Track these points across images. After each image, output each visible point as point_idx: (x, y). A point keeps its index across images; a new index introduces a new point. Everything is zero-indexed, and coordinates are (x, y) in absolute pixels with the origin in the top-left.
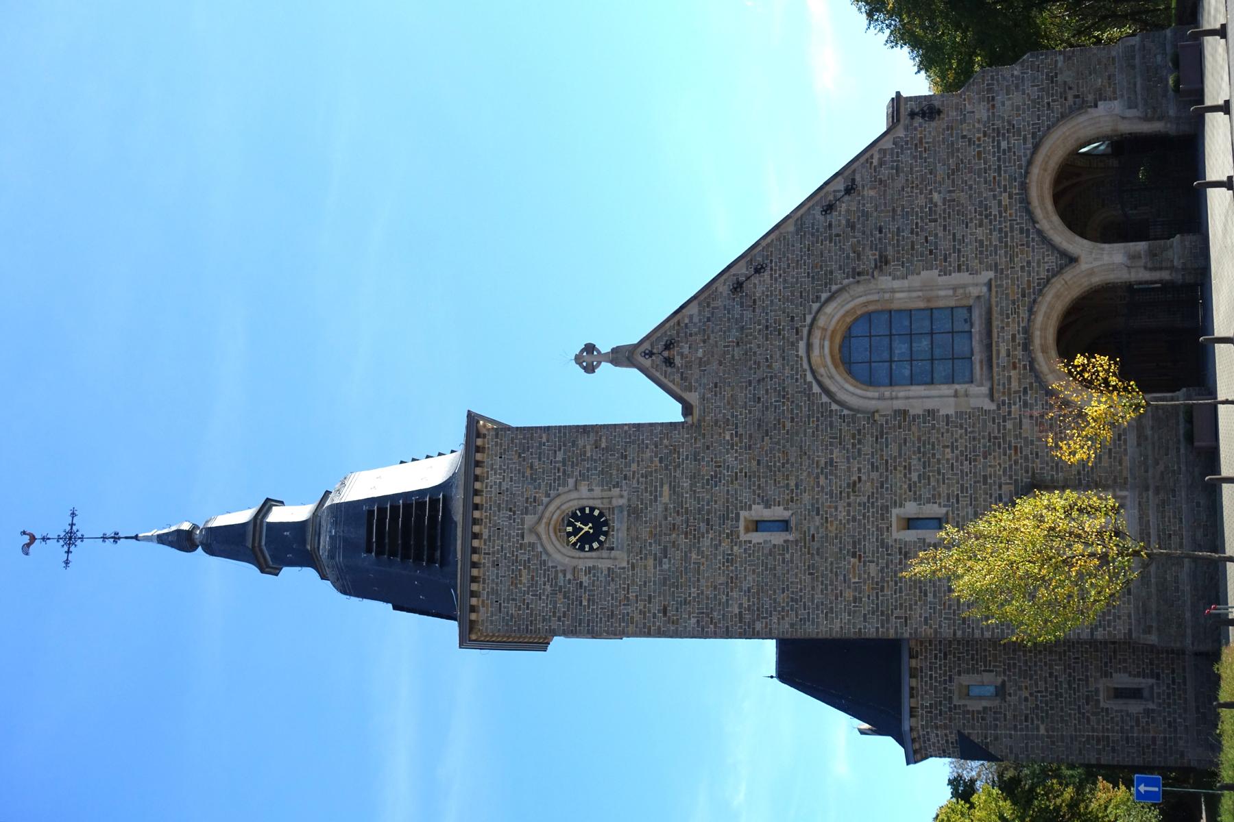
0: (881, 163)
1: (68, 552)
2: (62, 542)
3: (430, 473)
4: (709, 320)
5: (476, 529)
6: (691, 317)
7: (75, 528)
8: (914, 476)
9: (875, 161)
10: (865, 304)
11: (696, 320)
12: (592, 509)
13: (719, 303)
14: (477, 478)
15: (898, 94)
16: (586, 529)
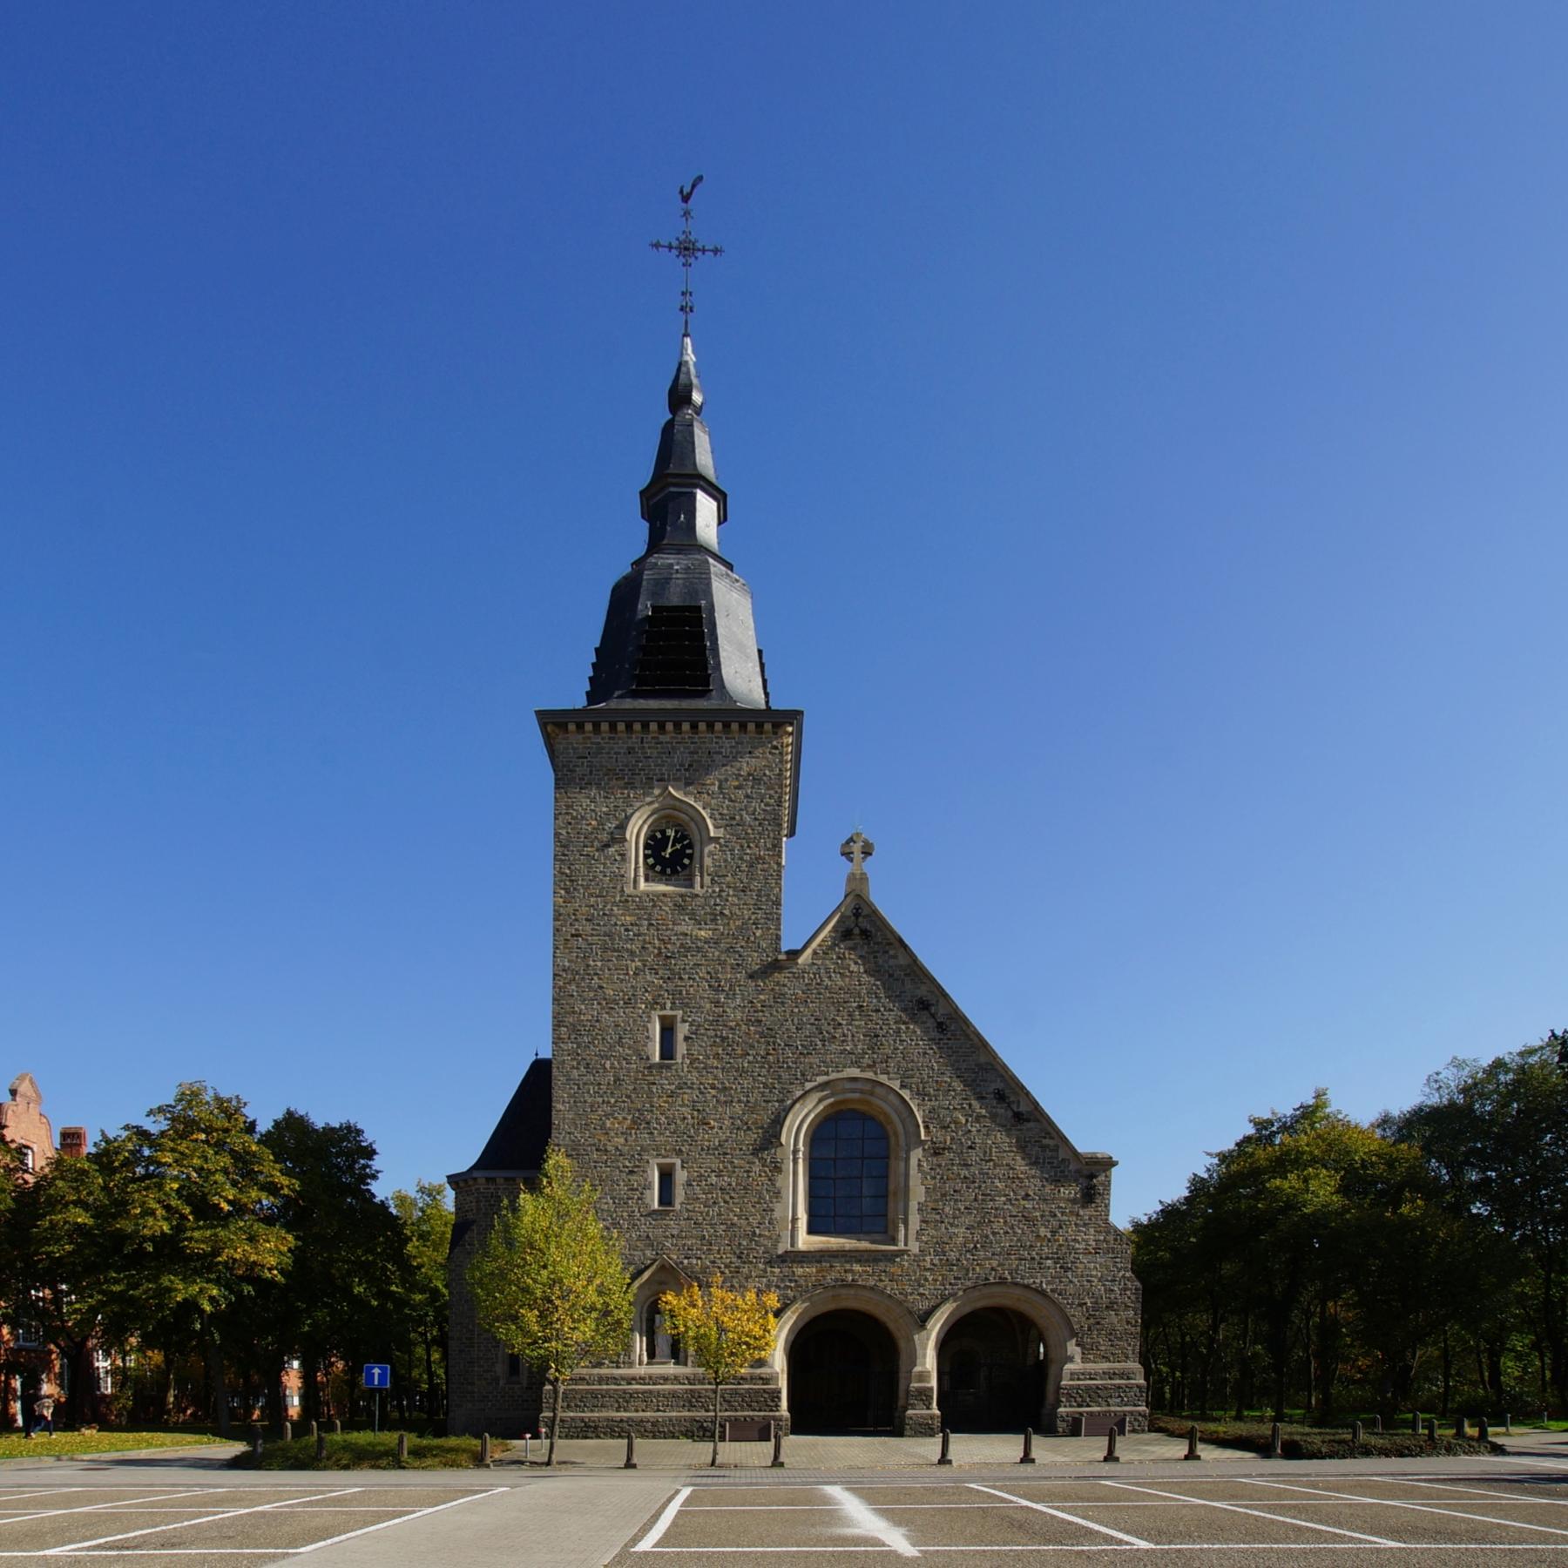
0: (1044, 1147)
1: (670, 247)
2: (691, 260)
3: (740, 674)
4: (891, 976)
5: (670, 726)
6: (895, 957)
7: (699, 254)
8: (714, 1179)
9: (1046, 1142)
10: (896, 1134)
11: (892, 962)
12: (690, 857)
13: (909, 985)
14: (727, 726)
15: (1116, 1164)
16: (669, 850)
